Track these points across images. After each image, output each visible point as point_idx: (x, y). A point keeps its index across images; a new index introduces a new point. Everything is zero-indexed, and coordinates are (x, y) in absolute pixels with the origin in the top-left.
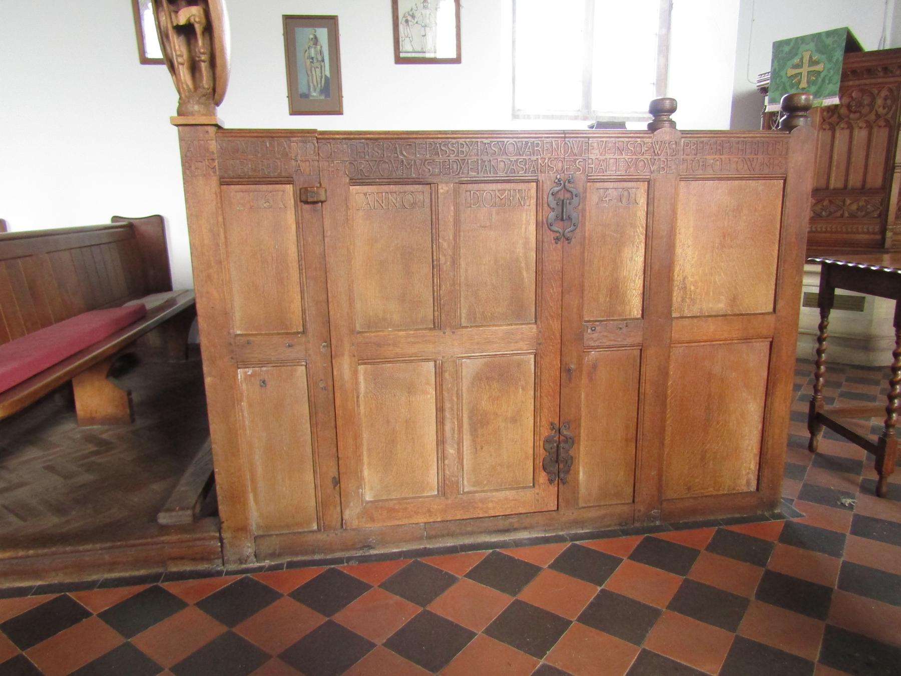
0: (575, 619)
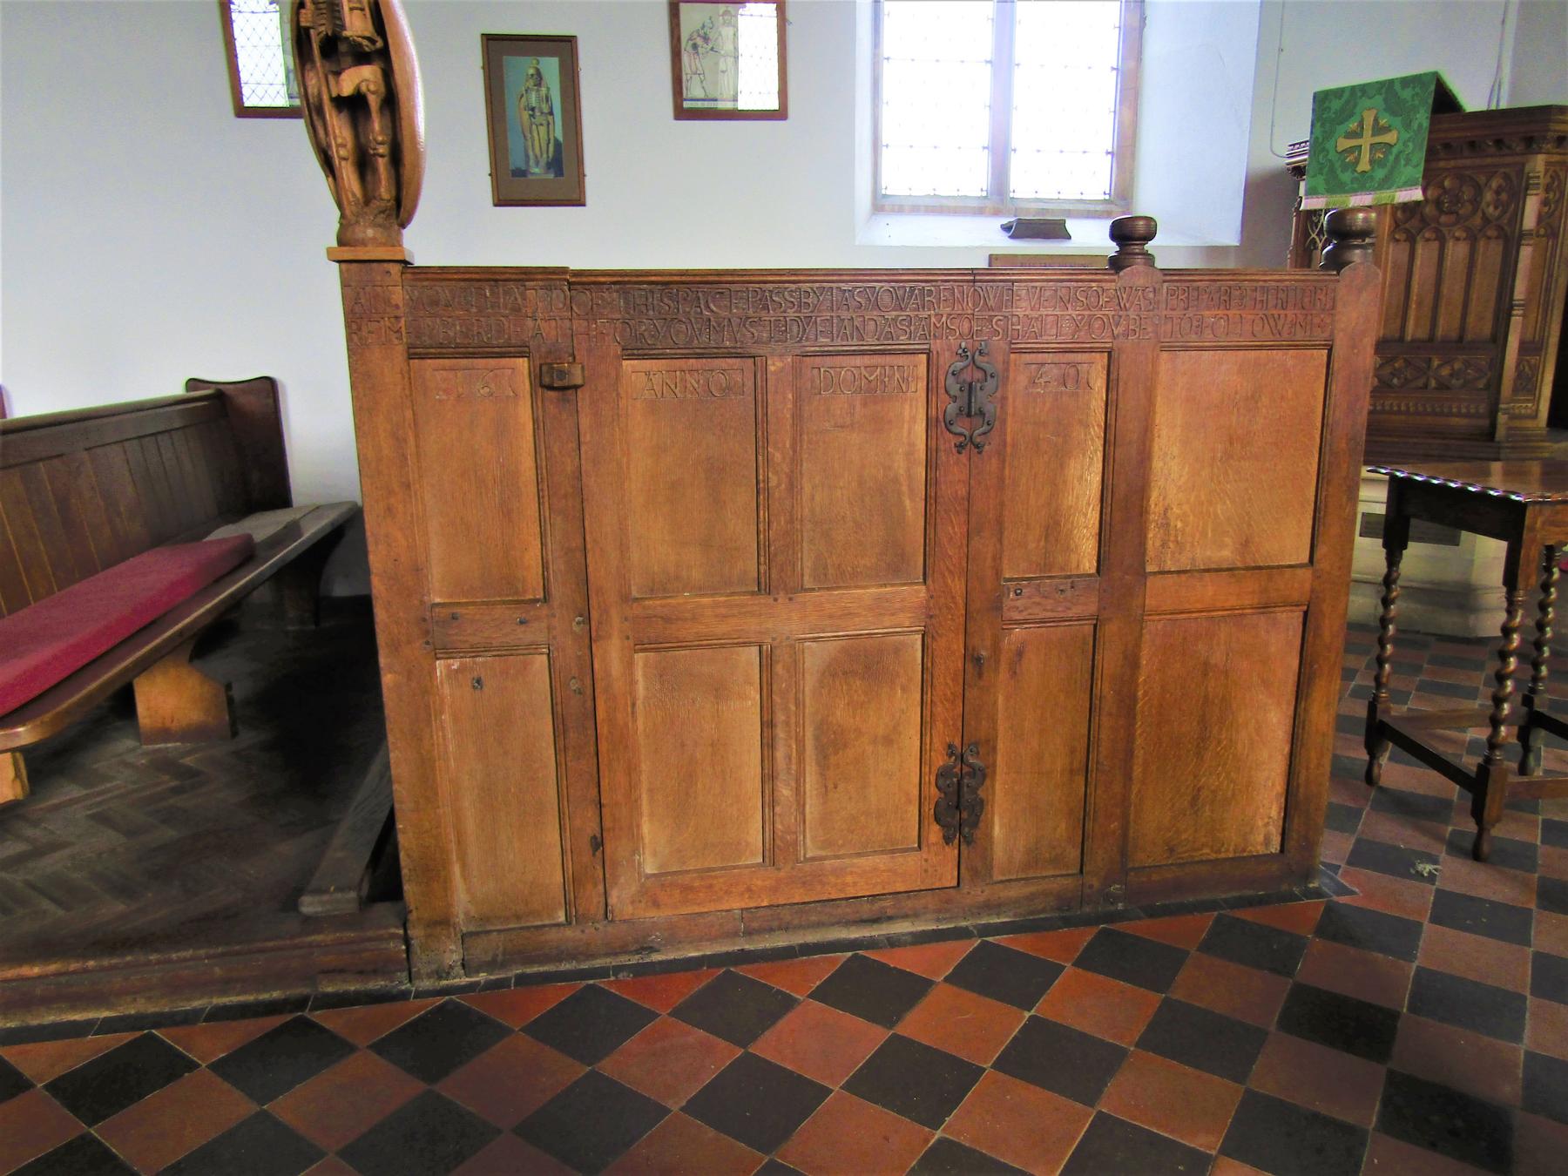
0: (990, 1065)
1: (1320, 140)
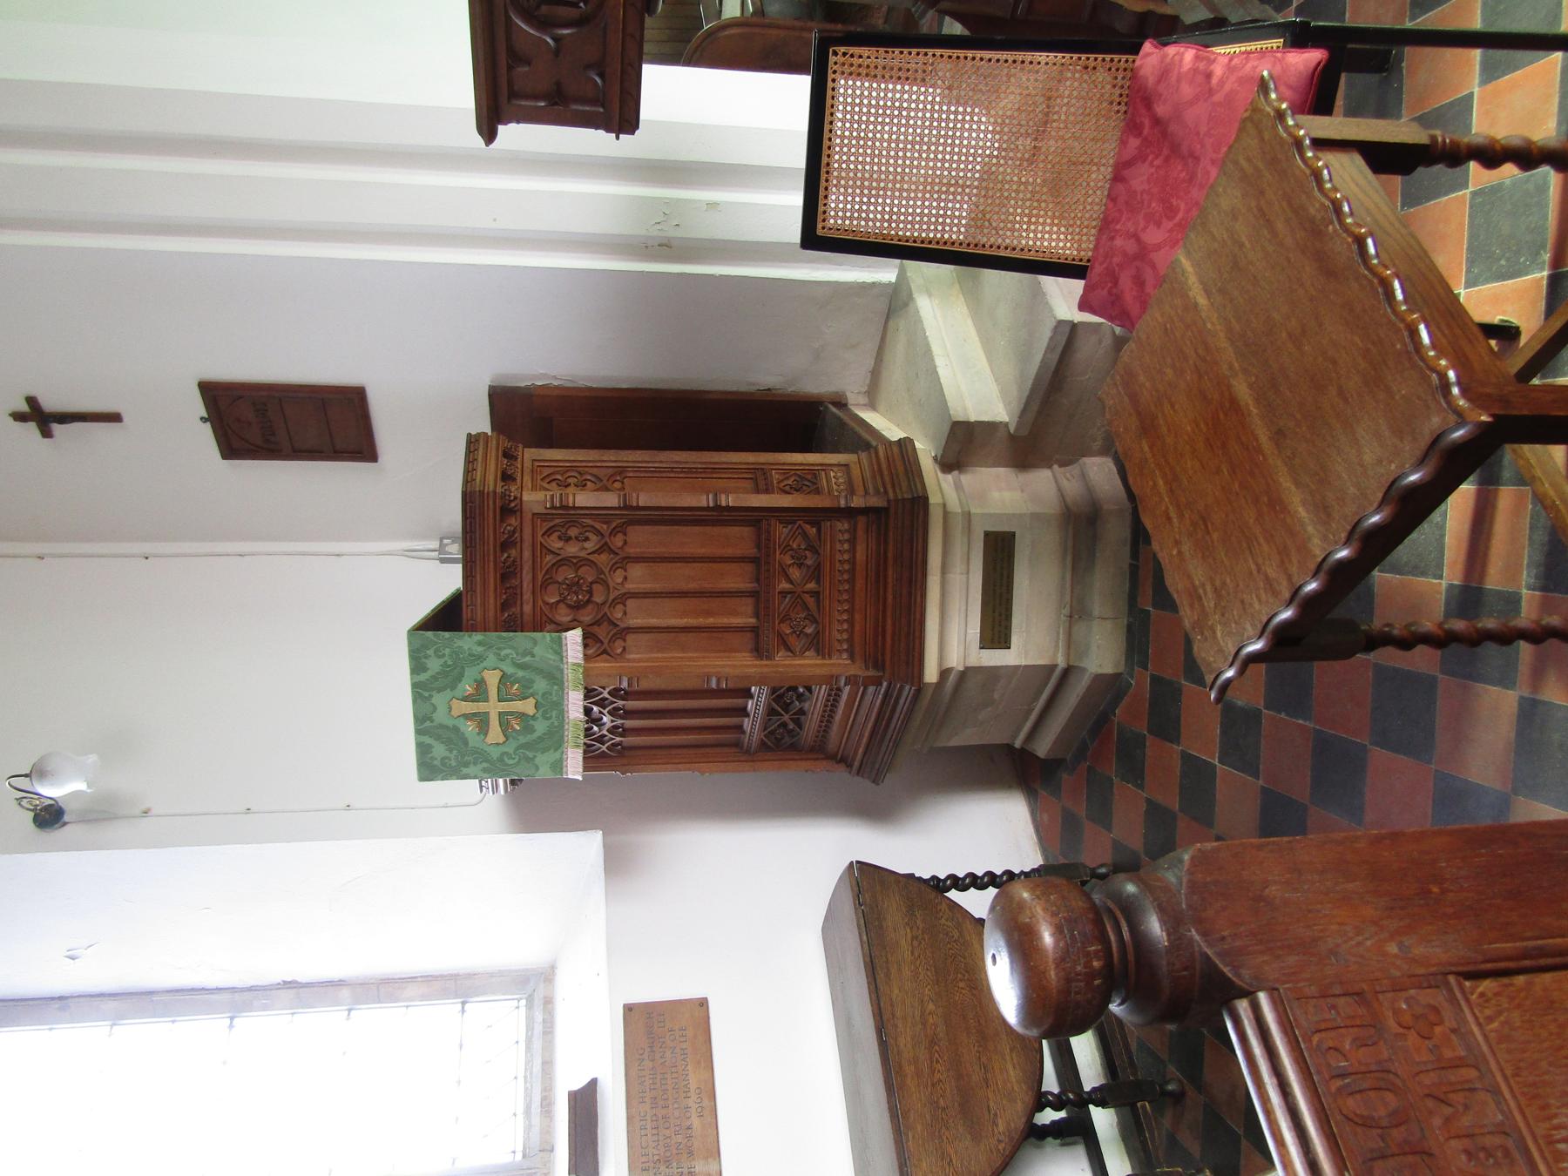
1: (485, 765)
